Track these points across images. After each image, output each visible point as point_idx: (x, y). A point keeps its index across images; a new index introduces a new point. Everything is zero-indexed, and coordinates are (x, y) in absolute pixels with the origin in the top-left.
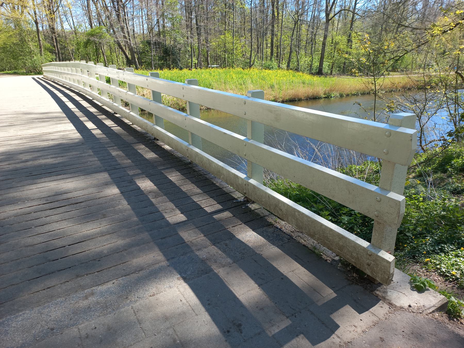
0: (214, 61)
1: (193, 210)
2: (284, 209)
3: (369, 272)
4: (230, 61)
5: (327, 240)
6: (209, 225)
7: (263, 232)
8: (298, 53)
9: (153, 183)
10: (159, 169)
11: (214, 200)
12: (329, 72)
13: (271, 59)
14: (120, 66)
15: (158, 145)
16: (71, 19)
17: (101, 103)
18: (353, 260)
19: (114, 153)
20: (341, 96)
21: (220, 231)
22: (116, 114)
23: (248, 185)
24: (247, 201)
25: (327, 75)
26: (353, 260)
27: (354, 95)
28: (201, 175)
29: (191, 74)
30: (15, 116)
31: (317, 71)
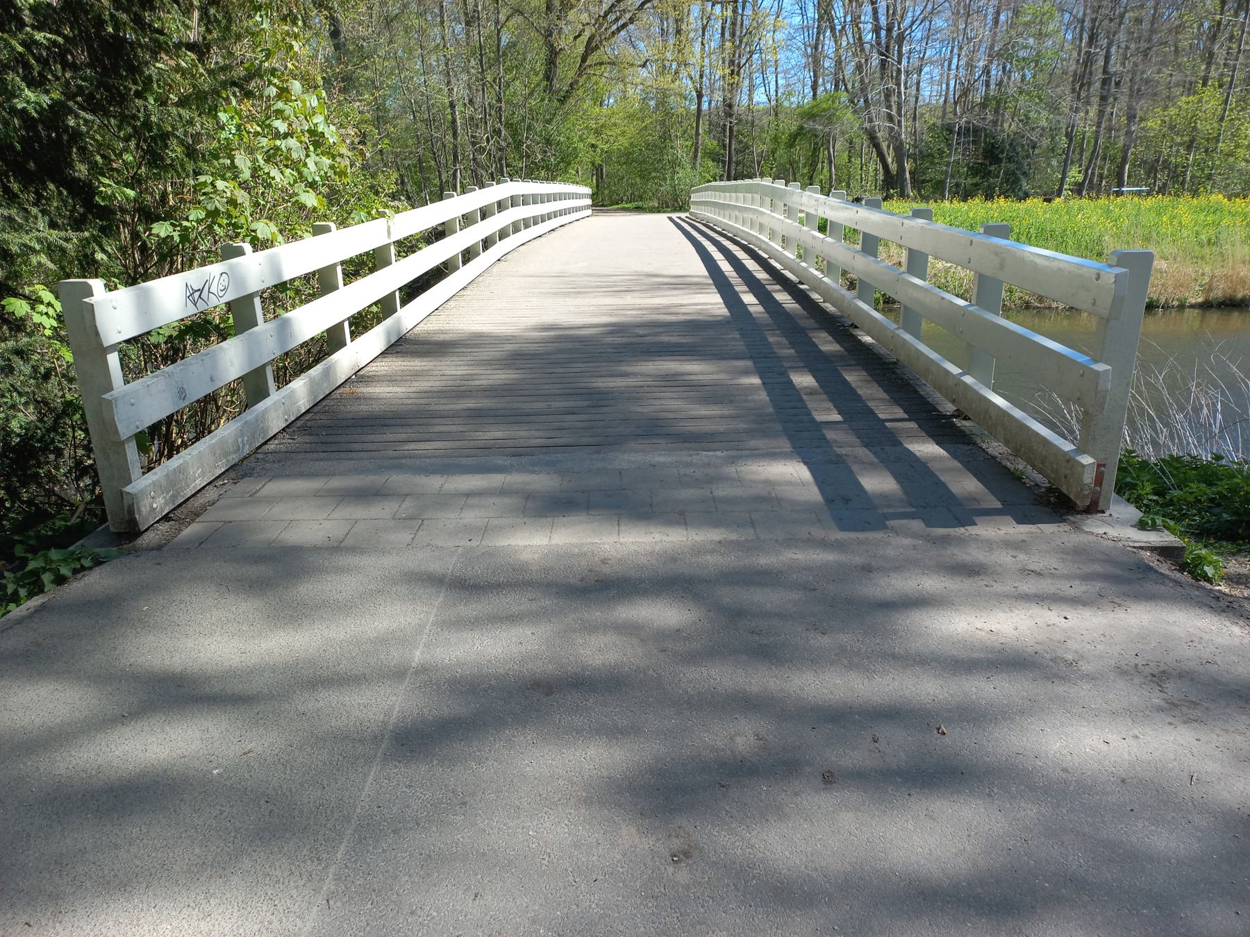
14: (865, 191)
16: (774, 79)
17: (780, 264)
19: (771, 339)
22: (802, 284)
29: (1045, 213)
30: (634, 277)
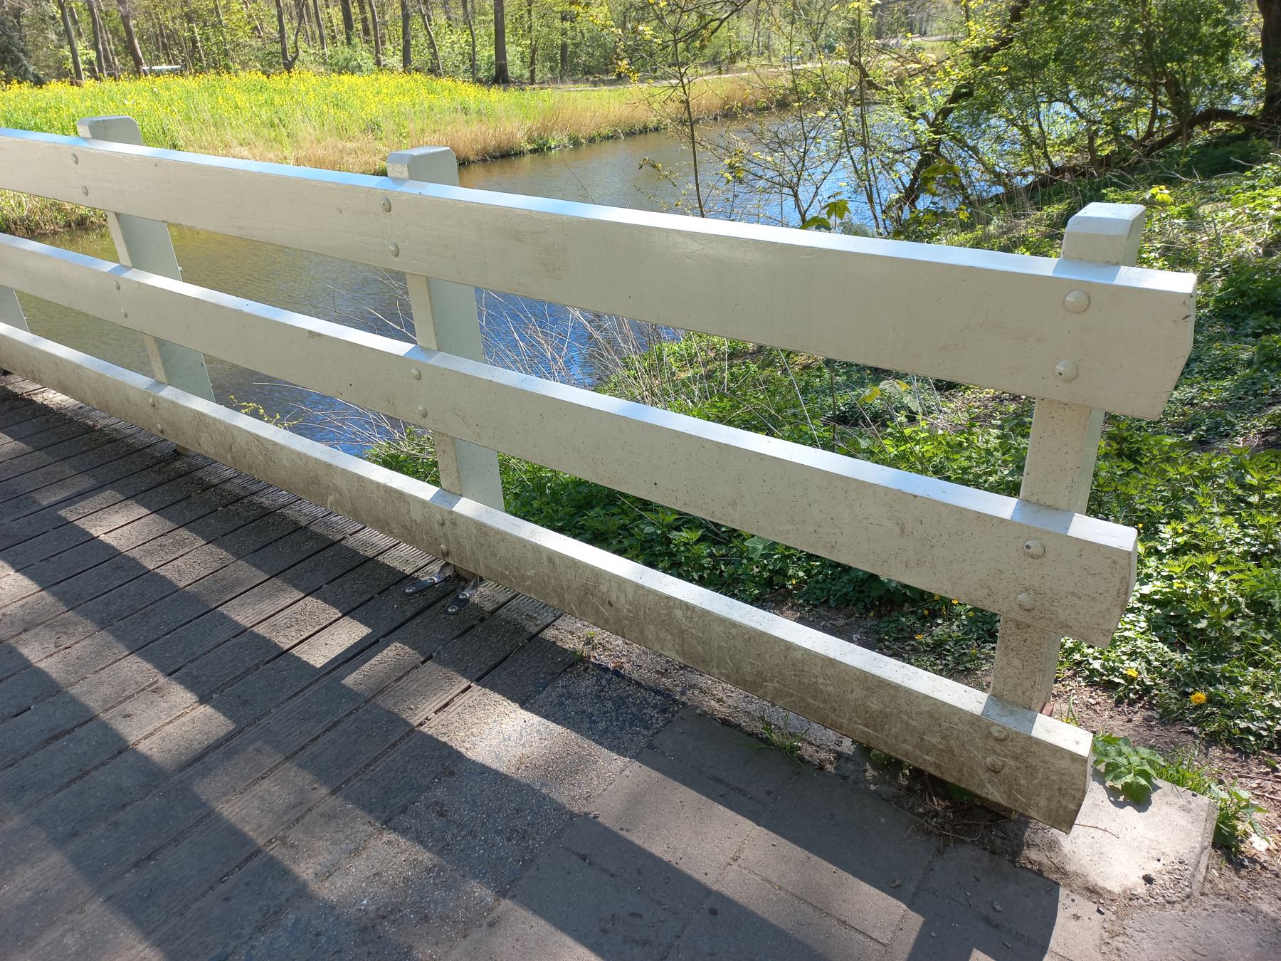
0: (158, 49)
1: (248, 672)
2: (623, 600)
3: (998, 795)
4: (214, 48)
5: (815, 697)
6: (340, 727)
7: (561, 704)
8: (427, 19)
9: (32, 577)
10: (45, 503)
11: (325, 601)
12: (527, 74)
13: (349, 39)
15: (15, 397)
18: (927, 758)
20: (576, 143)
21: (394, 745)
23: (454, 524)
24: (459, 579)
25: (522, 83)
26: (927, 758)
27: (608, 138)
28: (239, 499)
31: (493, 72)
